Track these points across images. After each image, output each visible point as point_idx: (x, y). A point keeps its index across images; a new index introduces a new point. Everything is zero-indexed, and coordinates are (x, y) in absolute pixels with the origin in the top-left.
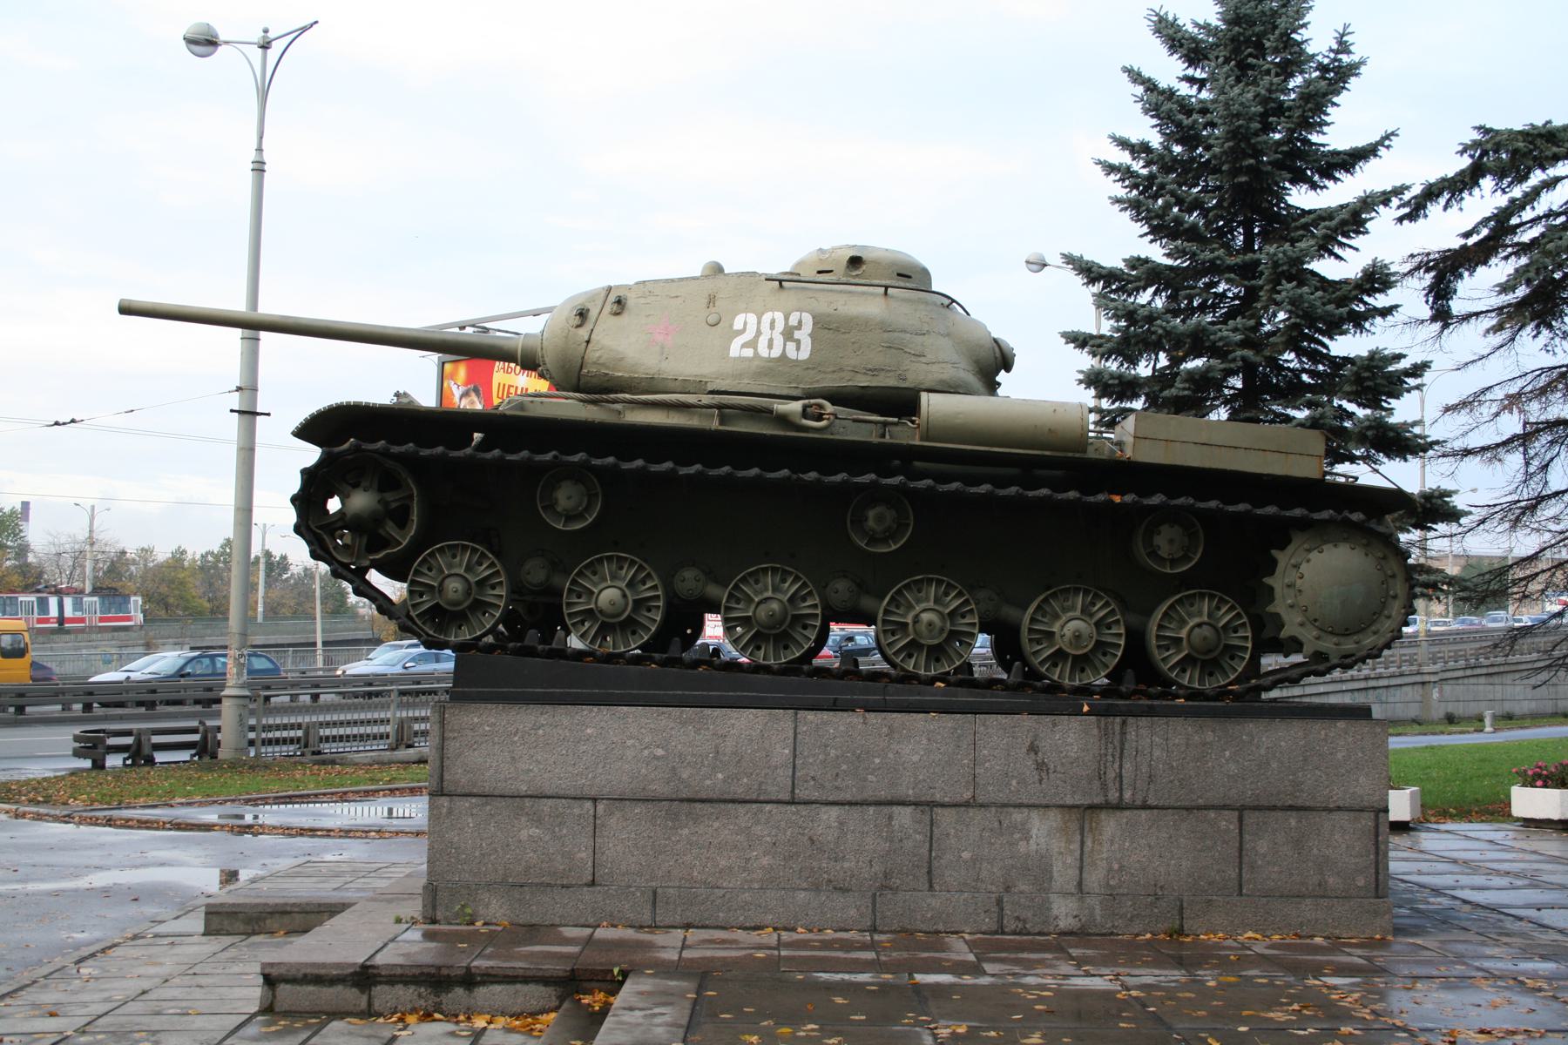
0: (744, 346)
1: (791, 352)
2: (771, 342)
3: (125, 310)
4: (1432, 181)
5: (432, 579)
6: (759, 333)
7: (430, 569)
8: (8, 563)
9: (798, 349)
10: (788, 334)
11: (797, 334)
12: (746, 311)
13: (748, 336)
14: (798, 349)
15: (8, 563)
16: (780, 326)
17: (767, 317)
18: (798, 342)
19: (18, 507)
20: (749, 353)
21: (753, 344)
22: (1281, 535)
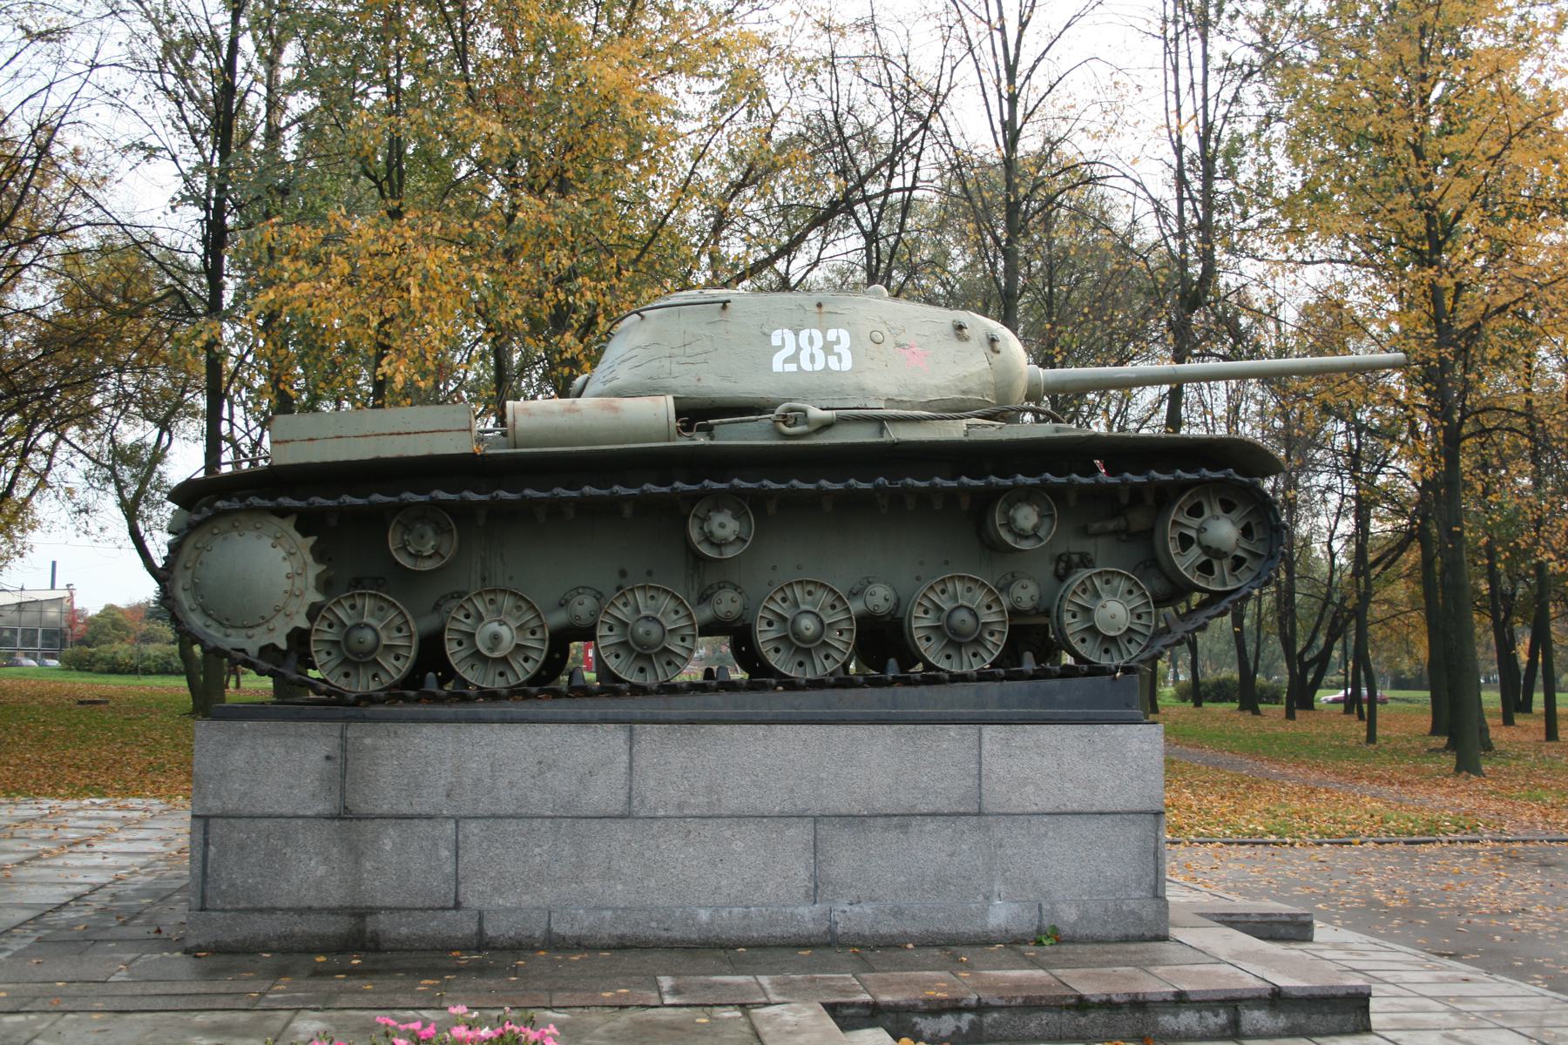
0: (786, 361)
1: (833, 363)
2: (812, 357)
3: (54, 564)
4: (122, 603)
5: (350, 617)
6: (799, 348)
7: (625, 605)
8: (1555, 237)
9: (840, 361)
10: (828, 348)
11: (836, 349)
12: (782, 326)
13: (789, 350)
14: (840, 361)
15: (1555, 237)
16: (819, 341)
17: (804, 334)
18: (839, 356)
19: (1298, 713)
20: (792, 367)
21: (794, 358)
22: (1164, 497)
